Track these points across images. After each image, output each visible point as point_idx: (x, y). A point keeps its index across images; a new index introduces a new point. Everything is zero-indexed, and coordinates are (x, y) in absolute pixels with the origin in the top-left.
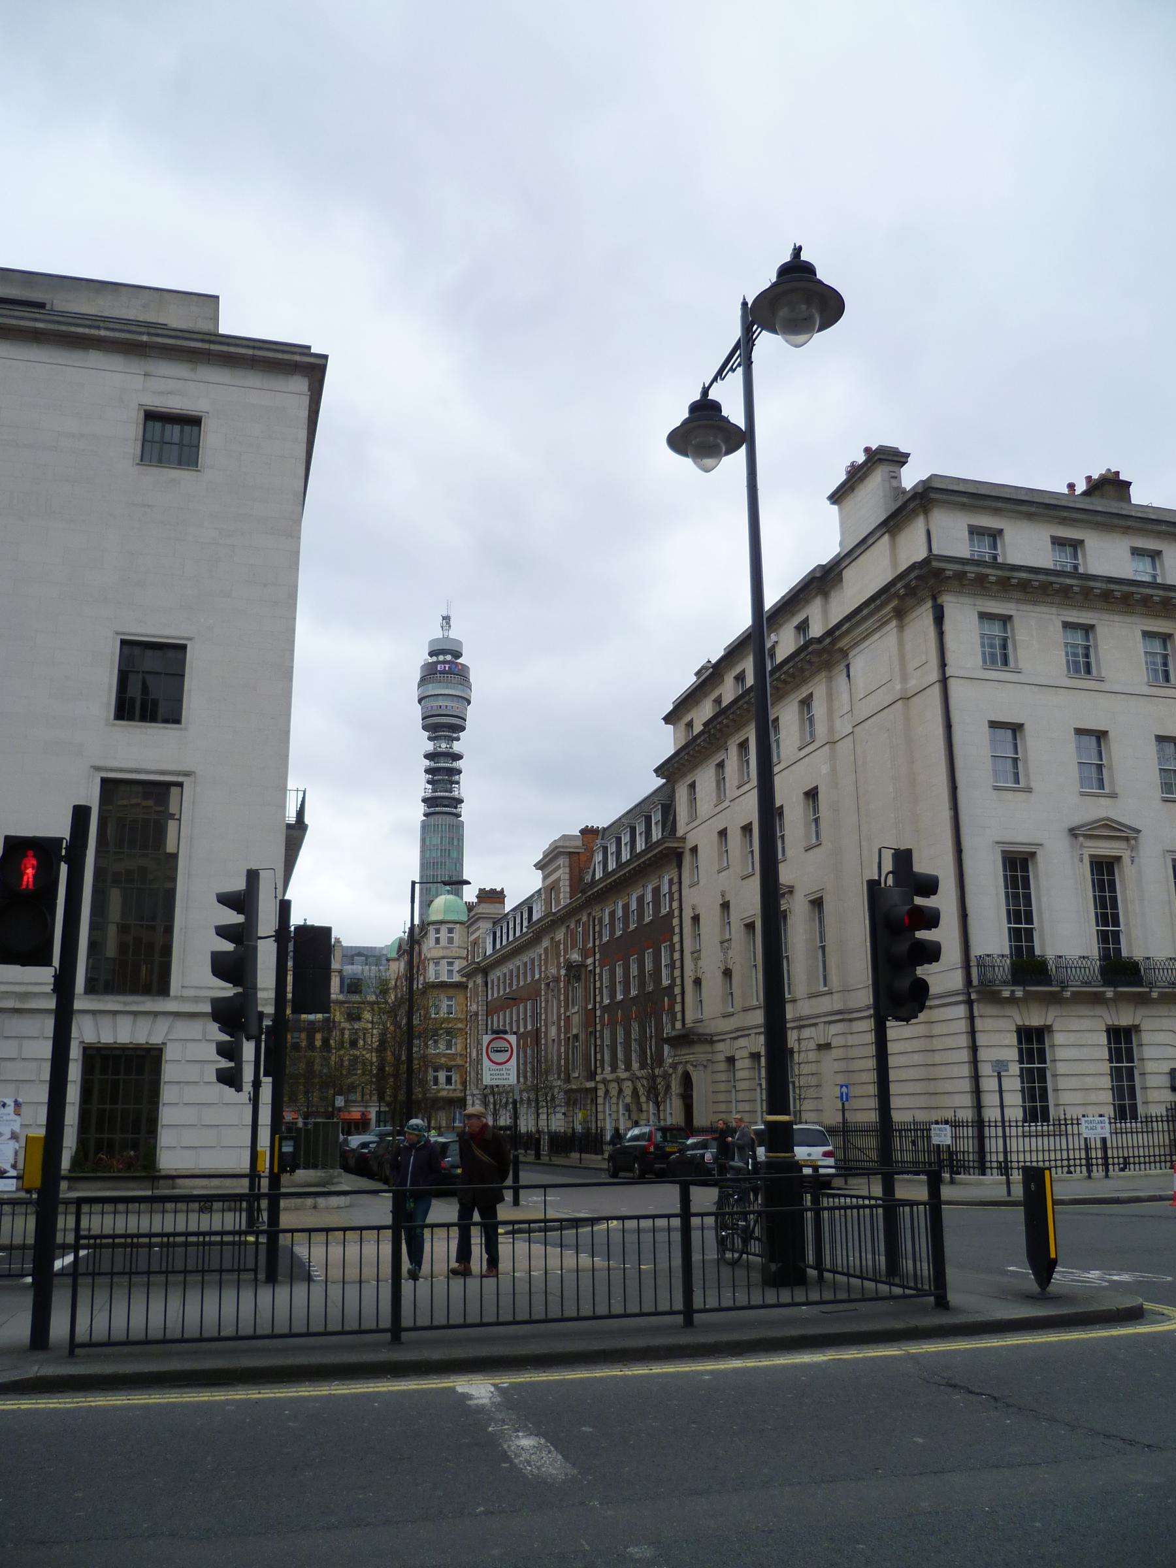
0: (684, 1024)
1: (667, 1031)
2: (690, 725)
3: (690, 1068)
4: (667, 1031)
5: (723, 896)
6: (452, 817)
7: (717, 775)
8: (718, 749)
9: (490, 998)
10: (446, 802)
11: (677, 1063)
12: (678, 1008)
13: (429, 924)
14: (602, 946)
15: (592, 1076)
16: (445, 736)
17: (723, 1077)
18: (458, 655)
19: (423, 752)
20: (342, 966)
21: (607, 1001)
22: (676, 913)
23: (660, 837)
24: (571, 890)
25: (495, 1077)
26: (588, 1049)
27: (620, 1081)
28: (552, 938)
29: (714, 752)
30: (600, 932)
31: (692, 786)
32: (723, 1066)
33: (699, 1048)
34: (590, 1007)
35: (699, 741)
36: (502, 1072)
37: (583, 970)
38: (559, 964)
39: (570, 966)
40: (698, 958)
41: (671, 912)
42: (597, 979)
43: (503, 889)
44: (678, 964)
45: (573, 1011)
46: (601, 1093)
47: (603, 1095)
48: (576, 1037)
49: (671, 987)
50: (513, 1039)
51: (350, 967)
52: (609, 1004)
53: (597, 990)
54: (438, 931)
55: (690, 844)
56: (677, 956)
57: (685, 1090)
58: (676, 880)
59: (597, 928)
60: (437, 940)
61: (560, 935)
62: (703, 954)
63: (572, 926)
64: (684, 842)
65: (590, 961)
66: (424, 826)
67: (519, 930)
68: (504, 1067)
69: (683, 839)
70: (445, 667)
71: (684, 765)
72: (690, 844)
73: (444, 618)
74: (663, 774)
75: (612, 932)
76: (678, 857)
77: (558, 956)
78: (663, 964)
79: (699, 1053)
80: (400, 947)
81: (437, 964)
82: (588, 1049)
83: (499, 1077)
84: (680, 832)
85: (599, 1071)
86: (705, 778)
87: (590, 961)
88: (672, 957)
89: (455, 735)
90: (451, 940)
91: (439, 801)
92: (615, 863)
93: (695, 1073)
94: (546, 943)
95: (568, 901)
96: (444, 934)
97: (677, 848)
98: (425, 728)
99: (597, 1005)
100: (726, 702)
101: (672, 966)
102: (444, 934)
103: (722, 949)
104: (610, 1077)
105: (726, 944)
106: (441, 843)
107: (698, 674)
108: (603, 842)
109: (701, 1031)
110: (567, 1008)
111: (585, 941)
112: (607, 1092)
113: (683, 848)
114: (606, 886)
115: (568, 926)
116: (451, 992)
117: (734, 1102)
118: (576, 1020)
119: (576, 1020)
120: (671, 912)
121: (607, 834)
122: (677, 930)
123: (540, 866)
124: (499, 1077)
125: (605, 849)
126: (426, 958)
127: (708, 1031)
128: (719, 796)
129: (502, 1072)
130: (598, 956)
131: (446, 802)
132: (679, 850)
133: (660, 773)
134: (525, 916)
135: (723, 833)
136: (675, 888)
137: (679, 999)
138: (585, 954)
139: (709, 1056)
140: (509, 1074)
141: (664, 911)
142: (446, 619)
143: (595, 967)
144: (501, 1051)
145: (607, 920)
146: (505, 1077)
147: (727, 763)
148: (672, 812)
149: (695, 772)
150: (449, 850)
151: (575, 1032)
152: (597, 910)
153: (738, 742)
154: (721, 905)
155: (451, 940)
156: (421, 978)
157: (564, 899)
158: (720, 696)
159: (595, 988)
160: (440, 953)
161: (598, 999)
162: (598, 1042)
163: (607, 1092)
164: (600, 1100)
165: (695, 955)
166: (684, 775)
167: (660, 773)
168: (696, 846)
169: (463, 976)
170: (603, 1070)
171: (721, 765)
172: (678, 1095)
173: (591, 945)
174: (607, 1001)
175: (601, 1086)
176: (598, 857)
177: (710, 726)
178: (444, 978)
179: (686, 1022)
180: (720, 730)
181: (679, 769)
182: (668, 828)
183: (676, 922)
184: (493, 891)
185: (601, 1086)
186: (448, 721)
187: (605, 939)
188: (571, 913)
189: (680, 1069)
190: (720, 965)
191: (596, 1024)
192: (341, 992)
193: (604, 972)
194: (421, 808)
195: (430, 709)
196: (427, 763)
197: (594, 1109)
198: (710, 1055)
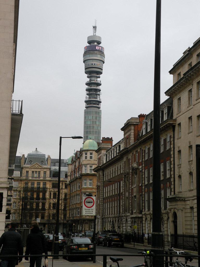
0: (174, 193)
1: (168, 195)
2: (179, 74)
3: (176, 211)
4: (168, 195)
5: (190, 143)
6: (96, 109)
7: (189, 95)
8: (189, 84)
9: (105, 180)
10: (94, 102)
11: (171, 208)
12: (172, 187)
13: (83, 151)
14: (145, 161)
15: (141, 212)
16: (94, 76)
17: (189, 215)
18: (99, 43)
19: (85, 83)
20: (51, 166)
21: (146, 183)
22: (172, 149)
23: (167, 119)
24: (134, 139)
25: (87, 212)
26: (140, 201)
27: (146, 215)
28: (127, 158)
29: (188, 86)
30: (145, 156)
31: (179, 99)
32: (189, 211)
33: (179, 203)
34: (140, 185)
35: (182, 81)
36: (90, 211)
37: (138, 170)
38: (129, 167)
39: (133, 169)
40: (180, 167)
41: (170, 149)
42: (143, 174)
43: (112, 138)
44: (172, 169)
45: (134, 186)
46: (144, 219)
47: (145, 220)
48: (135, 196)
49: (170, 178)
50: (94, 198)
51: (54, 167)
52: (147, 184)
53: (143, 179)
54: (86, 154)
55: (178, 122)
56: (172, 166)
57: (175, 219)
58: (172, 136)
59: (143, 154)
60: (86, 157)
61: (130, 156)
62: (182, 166)
63: (134, 153)
64: (176, 121)
65: (140, 167)
66: (86, 113)
67: (114, 154)
68: (91, 209)
69: (175, 120)
70: (99, 48)
71: (176, 91)
72: (178, 122)
73: (94, 27)
74: (168, 94)
75: (149, 156)
76: (174, 127)
77: (129, 165)
78: (167, 169)
79: (180, 205)
80: (72, 159)
81: (86, 167)
82: (140, 201)
83: (89, 212)
84: (174, 118)
85: (143, 210)
86: (184, 96)
87: (140, 167)
88: (170, 167)
89: (98, 76)
90: (91, 157)
91: (92, 102)
92: (150, 129)
93: (178, 213)
94: (125, 159)
95: (133, 143)
96: (89, 155)
97: (173, 124)
98: (86, 73)
99: (143, 184)
100: (193, 64)
101: (170, 170)
102: (89, 155)
103: (189, 164)
104: (147, 213)
105: (191, 162)
106: (92, 118)
107: (184, 53)
108: (146, 121)
109: (180, 196)
110: (132, 185)
111: (139, 160)
112: (146, 219)
113: (176, 124)
114: (146, 138)
115: (133, 153)
116: (91, 178)
117: (193, 225)
118: (135, 190)
119: (135, 190)
120: (170, 149)
121: (148, 117)
122: (172, 156)
123: (123, 129)
124: (89, 212)
125: (147, 123)
126: (82, 164)
127: (183, 196)
128: (189, 103)
129: (90, 211)
130: (143, 165)
131: (94, 102)
132: (174, 124)
133: (167, 94)
134: (118, 148)
135: (190, 118)
136: (172, 139)
137: (173, 183)
138: (139, 164)
139: (184, 206)
140: (93, 212)
141: (168, 148)
142: (95, 28)
143: (142, 170)
144: (90, 203)
145: (147, 151)
146: (91, 212)
147: (193, 90)
148: (171, 109)
149: (181, 94)
150: (95, 122)
151: (135, 194)
152: (144, 147)
153: (197, 82)
154: (189, 146)
155: (91, 157)
156: (80, 172)
157: (132, 142)
158: (191, 62)
159: (142, 178)
160: (87, 162)
161: (143, 182)
162: (143, 199)
163: (146, 219)
164: (144, 222)
165: (179, 166)
166: (176, 95)
167: (167, 94)
168: (180, 123)
169: (94, 171)
170: (145, 210)
171: (190, 91)
172: (172, 221)
173: (141, 161)
174: (146, 183)
175: (144, 216)
176: (144, 127)
177: (186, 75)
178: (89, 172)
179: (175, 193)
180: (190, 77)
181: (174, 92)
182: (170, 116)
183: (172, 153)
184: (108, 138)
185: (144, 216)
186: (95, 70)
187: (146, 158)
188: (135, 147)
189: (172, 210)
190: (188, 170)
191: (142, 192)
192: (50, 177)
193: (146, 171)
194: (84, 105)
195: (88, 65)
196: (87, 87)
197: (141, 225)
198: (184, 206)
